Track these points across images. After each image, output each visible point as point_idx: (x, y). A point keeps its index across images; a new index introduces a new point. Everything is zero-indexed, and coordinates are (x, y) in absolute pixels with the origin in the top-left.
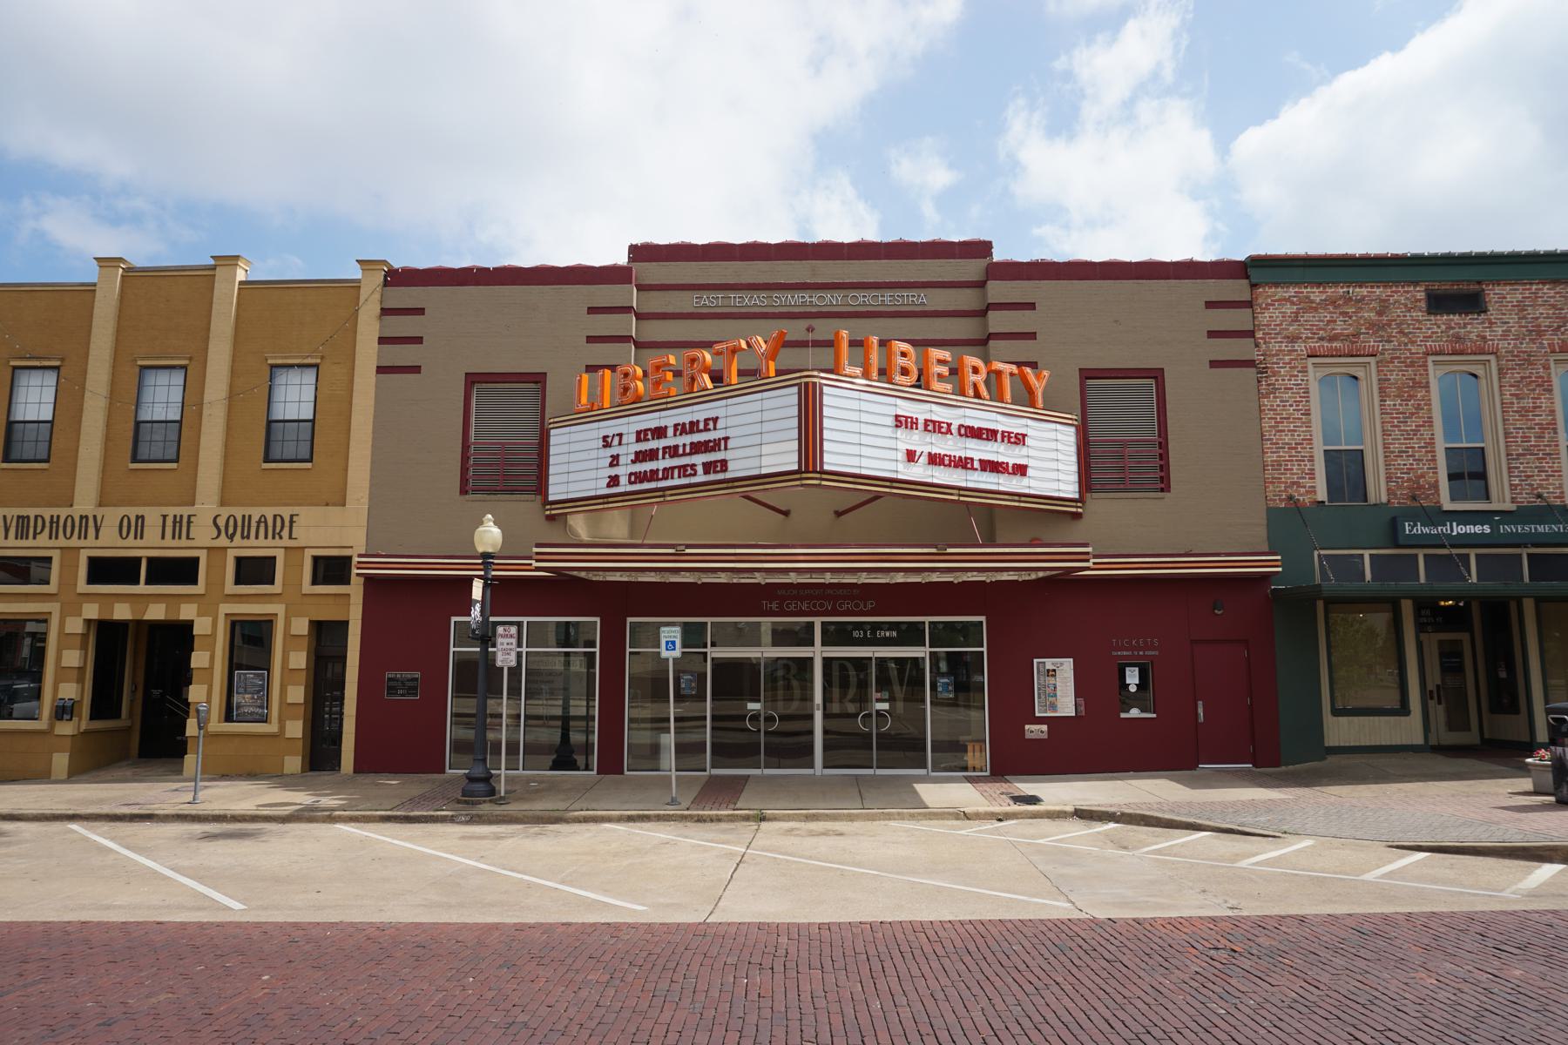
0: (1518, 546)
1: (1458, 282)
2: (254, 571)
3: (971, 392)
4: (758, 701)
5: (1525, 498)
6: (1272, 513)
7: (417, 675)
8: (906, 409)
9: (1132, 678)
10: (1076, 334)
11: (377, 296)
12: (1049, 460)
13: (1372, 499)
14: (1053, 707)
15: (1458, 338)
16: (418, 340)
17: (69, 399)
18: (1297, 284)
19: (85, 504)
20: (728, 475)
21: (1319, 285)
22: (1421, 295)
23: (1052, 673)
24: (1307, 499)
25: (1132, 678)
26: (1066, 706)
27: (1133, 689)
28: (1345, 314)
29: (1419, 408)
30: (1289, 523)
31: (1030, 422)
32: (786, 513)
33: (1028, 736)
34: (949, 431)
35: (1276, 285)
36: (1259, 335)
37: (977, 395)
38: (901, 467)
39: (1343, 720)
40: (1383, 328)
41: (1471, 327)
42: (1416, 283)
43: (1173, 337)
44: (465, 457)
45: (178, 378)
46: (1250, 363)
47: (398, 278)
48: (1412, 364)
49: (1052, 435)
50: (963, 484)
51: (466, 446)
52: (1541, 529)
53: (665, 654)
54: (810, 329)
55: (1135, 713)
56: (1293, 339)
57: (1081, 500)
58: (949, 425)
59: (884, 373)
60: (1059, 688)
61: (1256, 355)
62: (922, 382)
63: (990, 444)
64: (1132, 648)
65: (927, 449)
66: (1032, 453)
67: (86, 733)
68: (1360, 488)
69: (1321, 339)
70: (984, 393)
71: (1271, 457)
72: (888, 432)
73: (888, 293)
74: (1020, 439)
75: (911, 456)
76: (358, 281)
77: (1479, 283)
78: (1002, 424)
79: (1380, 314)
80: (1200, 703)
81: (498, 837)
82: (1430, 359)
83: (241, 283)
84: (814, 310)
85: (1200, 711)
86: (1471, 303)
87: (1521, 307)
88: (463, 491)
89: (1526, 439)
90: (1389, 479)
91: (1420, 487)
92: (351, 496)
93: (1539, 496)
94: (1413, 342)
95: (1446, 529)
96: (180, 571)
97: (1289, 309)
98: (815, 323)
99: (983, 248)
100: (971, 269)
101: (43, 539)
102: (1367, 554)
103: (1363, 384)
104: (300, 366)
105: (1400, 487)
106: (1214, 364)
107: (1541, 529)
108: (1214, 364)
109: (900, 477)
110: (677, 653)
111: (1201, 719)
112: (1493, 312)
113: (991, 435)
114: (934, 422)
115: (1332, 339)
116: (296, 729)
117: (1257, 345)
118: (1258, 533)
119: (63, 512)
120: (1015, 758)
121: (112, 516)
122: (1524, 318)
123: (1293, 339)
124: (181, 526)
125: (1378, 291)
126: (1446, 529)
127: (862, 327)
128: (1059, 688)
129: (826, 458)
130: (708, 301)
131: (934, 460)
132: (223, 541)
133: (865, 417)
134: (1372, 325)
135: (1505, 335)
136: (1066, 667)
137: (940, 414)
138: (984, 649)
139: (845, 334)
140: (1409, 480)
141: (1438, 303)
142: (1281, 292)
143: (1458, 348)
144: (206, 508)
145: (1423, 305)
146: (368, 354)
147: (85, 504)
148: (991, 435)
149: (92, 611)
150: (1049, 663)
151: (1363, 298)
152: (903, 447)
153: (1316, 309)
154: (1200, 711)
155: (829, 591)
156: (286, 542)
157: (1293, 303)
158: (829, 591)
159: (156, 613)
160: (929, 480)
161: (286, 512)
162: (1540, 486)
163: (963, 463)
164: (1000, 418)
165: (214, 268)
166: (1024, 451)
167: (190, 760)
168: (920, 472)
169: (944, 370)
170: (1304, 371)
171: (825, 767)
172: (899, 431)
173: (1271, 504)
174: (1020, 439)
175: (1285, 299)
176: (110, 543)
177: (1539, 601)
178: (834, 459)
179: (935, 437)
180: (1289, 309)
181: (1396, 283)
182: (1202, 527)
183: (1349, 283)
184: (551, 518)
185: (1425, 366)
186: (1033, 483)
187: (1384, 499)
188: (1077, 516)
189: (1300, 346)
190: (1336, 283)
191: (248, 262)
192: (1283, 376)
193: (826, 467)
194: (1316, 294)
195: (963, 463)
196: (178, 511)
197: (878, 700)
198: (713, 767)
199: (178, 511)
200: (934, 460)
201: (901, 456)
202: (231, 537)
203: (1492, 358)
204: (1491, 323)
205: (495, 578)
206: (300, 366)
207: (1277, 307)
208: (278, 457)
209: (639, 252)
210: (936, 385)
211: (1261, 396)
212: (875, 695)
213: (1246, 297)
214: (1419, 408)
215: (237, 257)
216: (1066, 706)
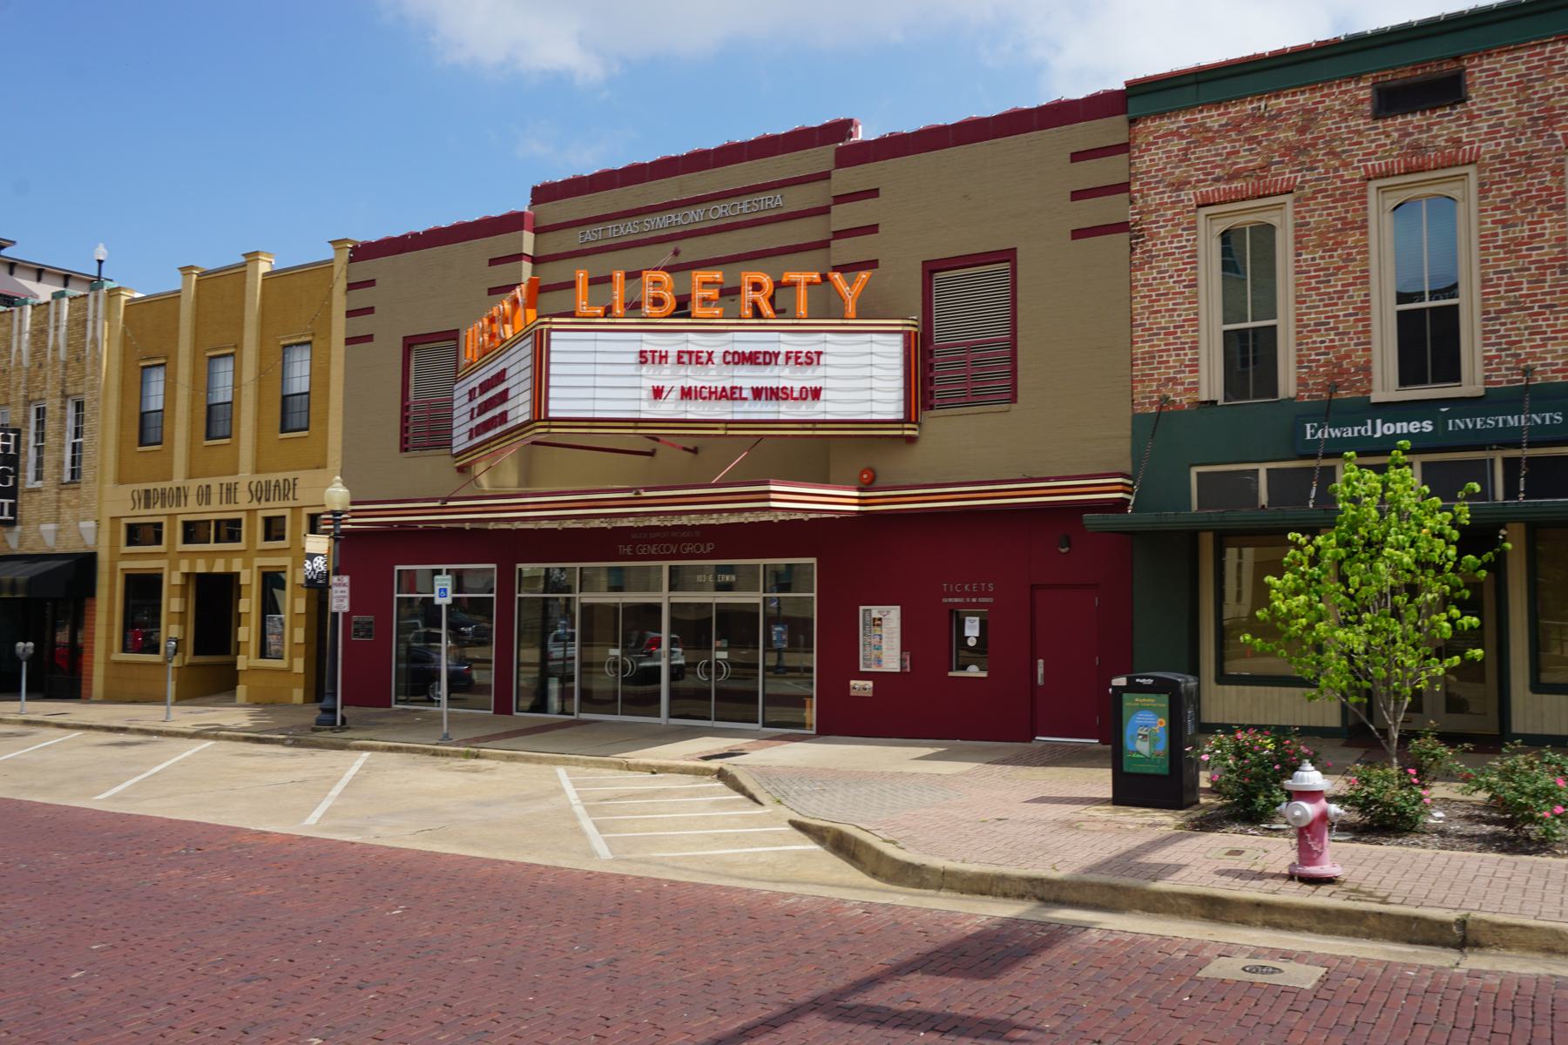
0: (1481, 448)
1: (1423, 64)
2: (273, 528)
3: (748, 312)
4: (616, 647)
5: (1505, 377)
6: (1137, 419)
7: (371, 618)
8: (652, 342)
9: (972, 629)
10: (922, 217)
11: (344, 273)
12: (860, 375)
13: (1282, 395)
14: (879, 661)
15: (1417, 148)
16: (1077, 195)
17: (320, 374)
18: (1188, 109)
19: (179, 480)
20: (510, 425)
21: (1218, 104)
22: (1365, 94)
23: (878, 622)
24: (1185, 400)
25: (972, 629)
26: (891, 660)
27: (972, 643)
28: (1250, 140)
29: (1349, 258)
30: (1162, 431)
31: (829, 337)
32: (695, 451)
33: (853, 693)
34: (788, 356)
35: (1161, 115)
36: (1135, 187)
37: (757, 313)
38: (645, 406)
39: (1231, 690)
40: (1304, 150)
41: (1435, 128)
42: (1358, 77)
43: (1020, 201)
44: (405, 419)
45: (230, 360)
46: (1122, 227)
47: (362, 252)
48: (1343, 198)
49: (866, 348)
50: (729, 417)
51: (405, 408)
52: (1513, 421)
53: (438, 601)
54: (676, 253)
55: (973, 671)
56: (1178, 186)
57: (907, 420)
58: (710, 354)
59: (634, 307)
60: (884, 641)
61: (1131, 216)
62: (683, 307)
63: (769, 368)
64: (962, 594)
65: (678, 384)
66: (830, 371)
67: (190, 665)
68: (1268, 382)
69: (1217, 180)
70: (767, 310)
71: (1141, 348)
72: (632, 370)
73: (746, 200)
74: (812, 359)
75: (658, 393)
76: (331, 261)
77: (1457, 58)
78: (785, 343)
79: (1302, 131)
80: (1041, 662)
81: (278, 755)
82: (1373, 185)
83: (265, 274)
84: (679, 230)
85: (1041, 671)
86: (1446, 91)
87: (1524, 84)
88: (404, 449)
89: (1514, 286)
90: (1300, 363)
91: (1343, 372)
92: (241, 468)
93: (1528, 371)
94: (1346, 165)
95: (1365, 430)
96: (230, 530)
97: (1176, 145)
98: (682, 245)
99: (842, 128)
100: (821, 157)
101: (158, 509)
102: (1262, 469)
103: (1461, 207)
104: (297, 344)
105: (1312, 374)
106: (1078, 234)
107: (1513, 421)
108: (1078, 234)
109: (643, 416)
110: (448, 600)
111: (1040, 681)
112: (1476, 100)
113: (770, 358)
114: (690, 353)
115: (1231, 178)
116: (299, 666)
117: (1132, 202)
118: (1119, 451)
119: (167, 485)
120: (845, 719)
121: (193, 485)
122: (1528, 100)
123: (1178, 186)
124: (230, 492)
125: (1301, 98)
126: (1365, 430)
127: (600, 264)
128: (884, 641)
129: (552, 405)
130: (722, 211)
131: (686, 393)
132: (255, 505)
133: (600, 358)
134: (1290, 150)
135: (1492, 133)
136: (892, 617)
137: (696, 342)
138: (815, 595)
139: (582, 275)
140: (1327, 363)
141: (1390, 102)
142: (1168, 124)
143: (1416, 163)
144: (245, 477)
145: (1367, 107)
146: (340, 327)
147: (179, 480)
148: (770, 358)
149: (185, 566)
150: (876, 611)
151: (1280, 111)
152: (649, 384)
153: (1212, 140)
154: (1041, 671)
155: (674, 534)
156: (291, 503)
157: (1182, 137)
158: (674, 534)
159: (219, 567)
160: (682, 416)
161: (290, 476)
162: (1532, 356)
163: (731, 394)
164: (783, 337)
165: (244, 265)
166: (820, 371)
167: (241, 690)
168: (670, 408)
169: (713, 293)
170: (1192, 227)
171: (671, 716)
172: (644, 369)
173: (1139, 409)
174: (812, 359)
175: (1172, 133)
176: (192, 510)
177: (1535, 530)
178: (558, 407)
179: (690, 370)
180: (1176, 145)
181: (1328, 82)
182: (1053, 445)
183: (1260, 95)
184: (461, 469)
185: (1363, 197)
186: (830, 407)
187: (1292, 394)
188: (911, 440)
189: (1188, 195)
190: (1241, 99)
191: (269, 255)
192: (1164, 238)
193: (551, 415)
194: (1214, 119)
195: (731, 394)
196: (226, 480)
197: (718, 649)
198: (580, 711)
199: (226, 480)
200: (686, 393)
201: (646, 394)
202: (259, 500)
203: (1471, 169)
204: (1471, 117)
205: (344, 532)
206: (297, 344)
207: (1160, 146)
208: (296, 426)
209: (542, 194)
210: (697, 310)
211: (1133, 268)
212: (715, 643)
213: (1122, 138)
214: (1349, 258)
215: (256, 253)
216: (891, 660)
